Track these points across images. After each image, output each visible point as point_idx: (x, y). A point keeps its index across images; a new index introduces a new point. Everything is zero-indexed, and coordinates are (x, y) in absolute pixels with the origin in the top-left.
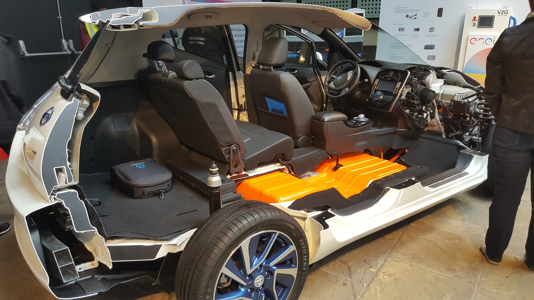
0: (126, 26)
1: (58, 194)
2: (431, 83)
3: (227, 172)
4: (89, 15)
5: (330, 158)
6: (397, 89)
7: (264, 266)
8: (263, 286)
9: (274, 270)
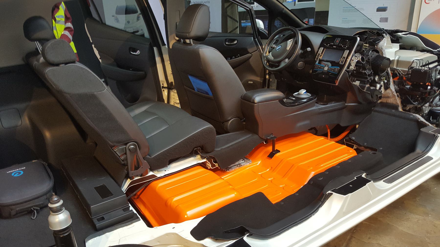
2: (384, 49)
5: (265, 143)
6: (344, 59)
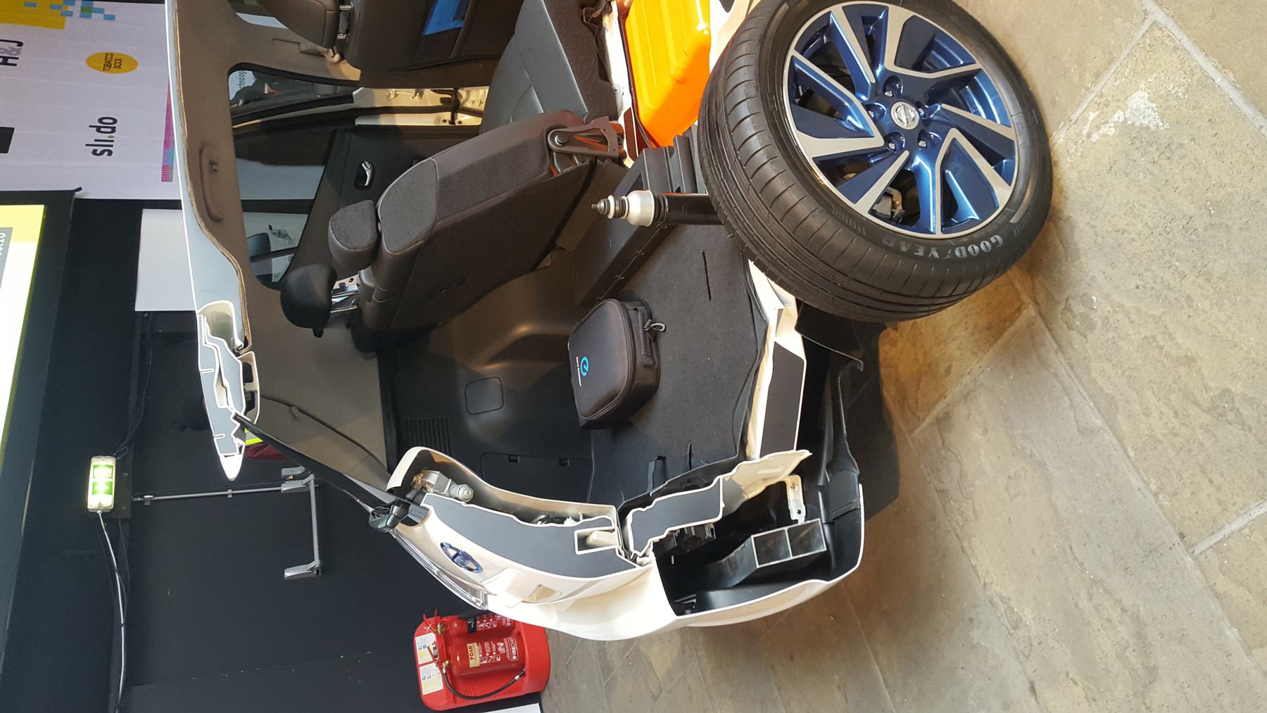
0: (248, 378)
1: (635, 550)
3: (617, 166)
4: (223, 460)
7: (871, 98)
8: (918, 105)
9: (885, 71)
